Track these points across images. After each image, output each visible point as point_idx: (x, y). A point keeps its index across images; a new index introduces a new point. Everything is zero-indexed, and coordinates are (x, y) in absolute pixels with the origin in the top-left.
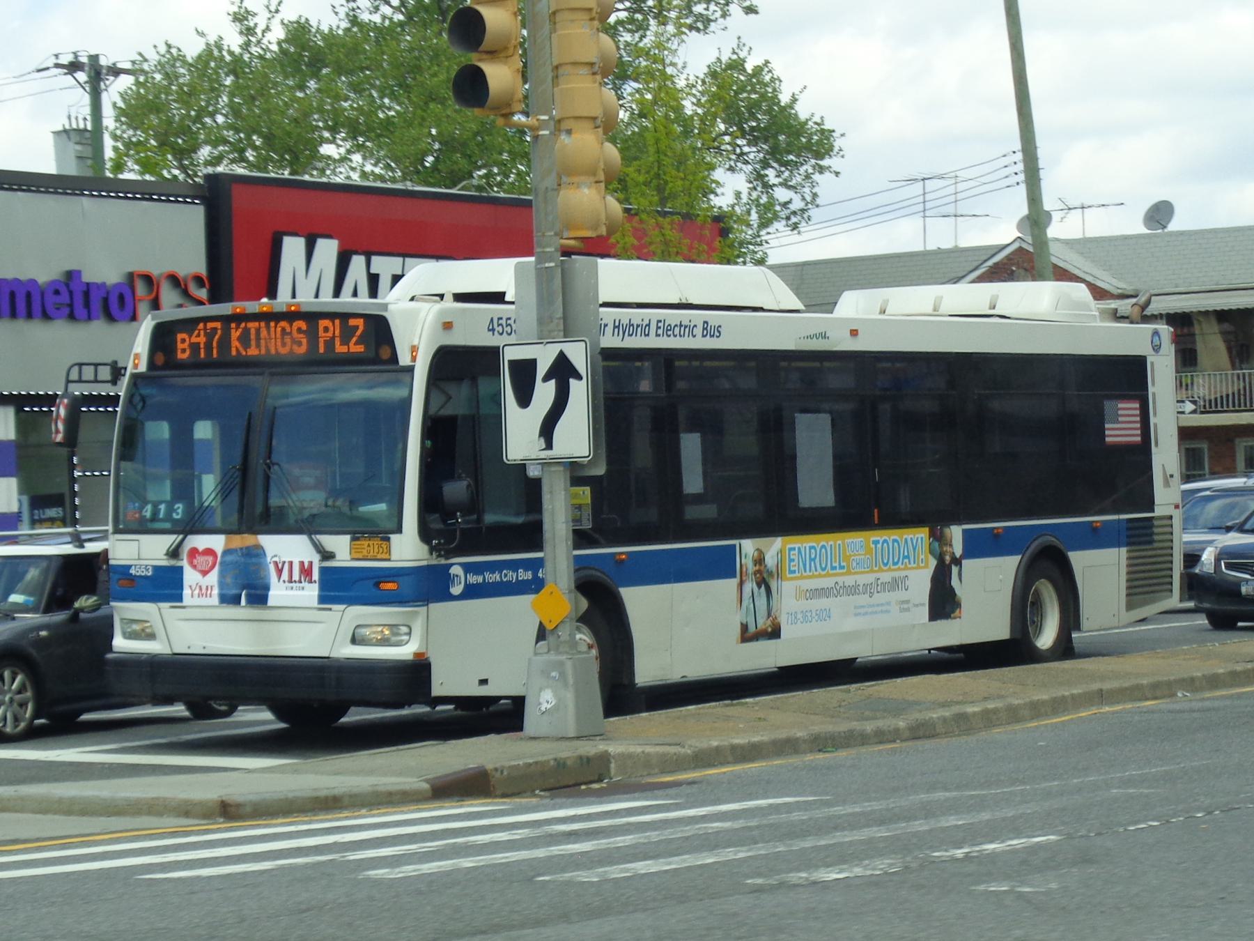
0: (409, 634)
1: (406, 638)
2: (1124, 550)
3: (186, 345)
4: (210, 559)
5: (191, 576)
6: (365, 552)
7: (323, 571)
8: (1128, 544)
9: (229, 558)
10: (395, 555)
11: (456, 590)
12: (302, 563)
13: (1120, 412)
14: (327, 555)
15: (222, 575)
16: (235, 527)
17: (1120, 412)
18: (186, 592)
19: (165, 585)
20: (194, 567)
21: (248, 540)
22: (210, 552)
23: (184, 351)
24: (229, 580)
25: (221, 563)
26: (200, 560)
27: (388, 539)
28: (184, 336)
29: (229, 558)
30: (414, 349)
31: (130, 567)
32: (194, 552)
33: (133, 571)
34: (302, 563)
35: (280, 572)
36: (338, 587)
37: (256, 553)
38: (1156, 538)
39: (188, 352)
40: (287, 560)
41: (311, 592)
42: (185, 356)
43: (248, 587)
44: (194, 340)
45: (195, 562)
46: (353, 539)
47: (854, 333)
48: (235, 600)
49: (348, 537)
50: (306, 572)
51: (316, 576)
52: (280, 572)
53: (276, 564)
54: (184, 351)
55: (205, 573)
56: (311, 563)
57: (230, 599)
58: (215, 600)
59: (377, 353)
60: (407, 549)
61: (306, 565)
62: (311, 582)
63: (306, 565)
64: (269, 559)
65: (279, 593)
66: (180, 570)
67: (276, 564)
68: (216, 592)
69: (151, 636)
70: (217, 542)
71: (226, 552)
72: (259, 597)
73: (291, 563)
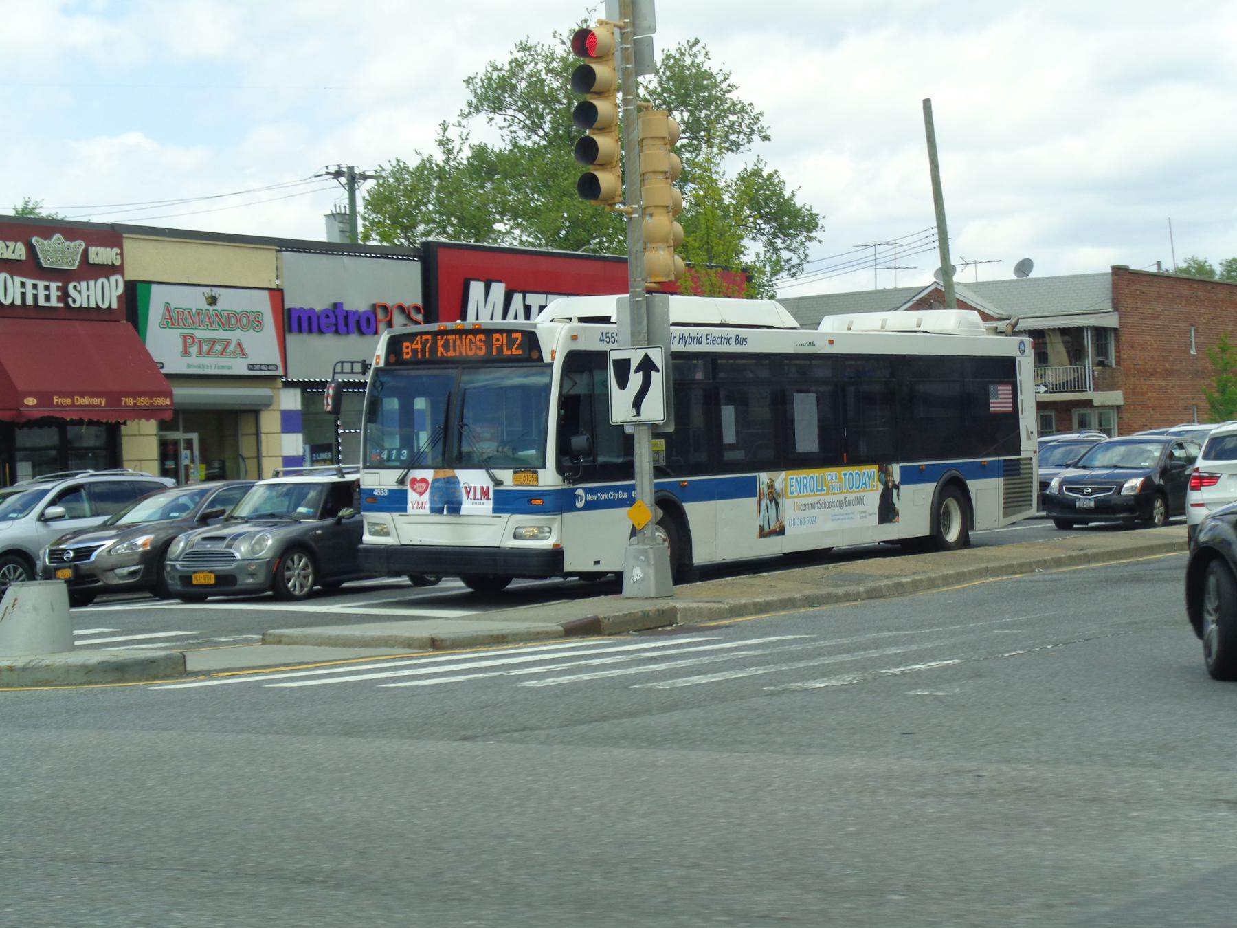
2: (1001, 479)
4: (424, 485)
5: (412, 496)
9: (436, 484)
11: (580, 504)
14: (498, 483)
15: (432, 495)
18: (409, 506)
19: (396, 502)
21: (448, 473)
22: (424, 480)
24: (436, 498)
26: (417, 485)
29: (436, 484)
30: (553, 352)
32: (414, 481)
35: (468, 493)
36: (505, 502)
37: (453, 481)
41: (488, 506)
43: (448, 502)
44: (414, 346)
48: (440, 511)
50: (485, 493)
51: (491, 495)
52: (468, 493)
55: (421, 494)
57: (437, 510)
58: (427, 511)
60: (549, 478)
65: (467, 506)
68: (428, 506)
69: (387, 534)
70: (429, 474)
71: (434, 481)
72: (455, 509)
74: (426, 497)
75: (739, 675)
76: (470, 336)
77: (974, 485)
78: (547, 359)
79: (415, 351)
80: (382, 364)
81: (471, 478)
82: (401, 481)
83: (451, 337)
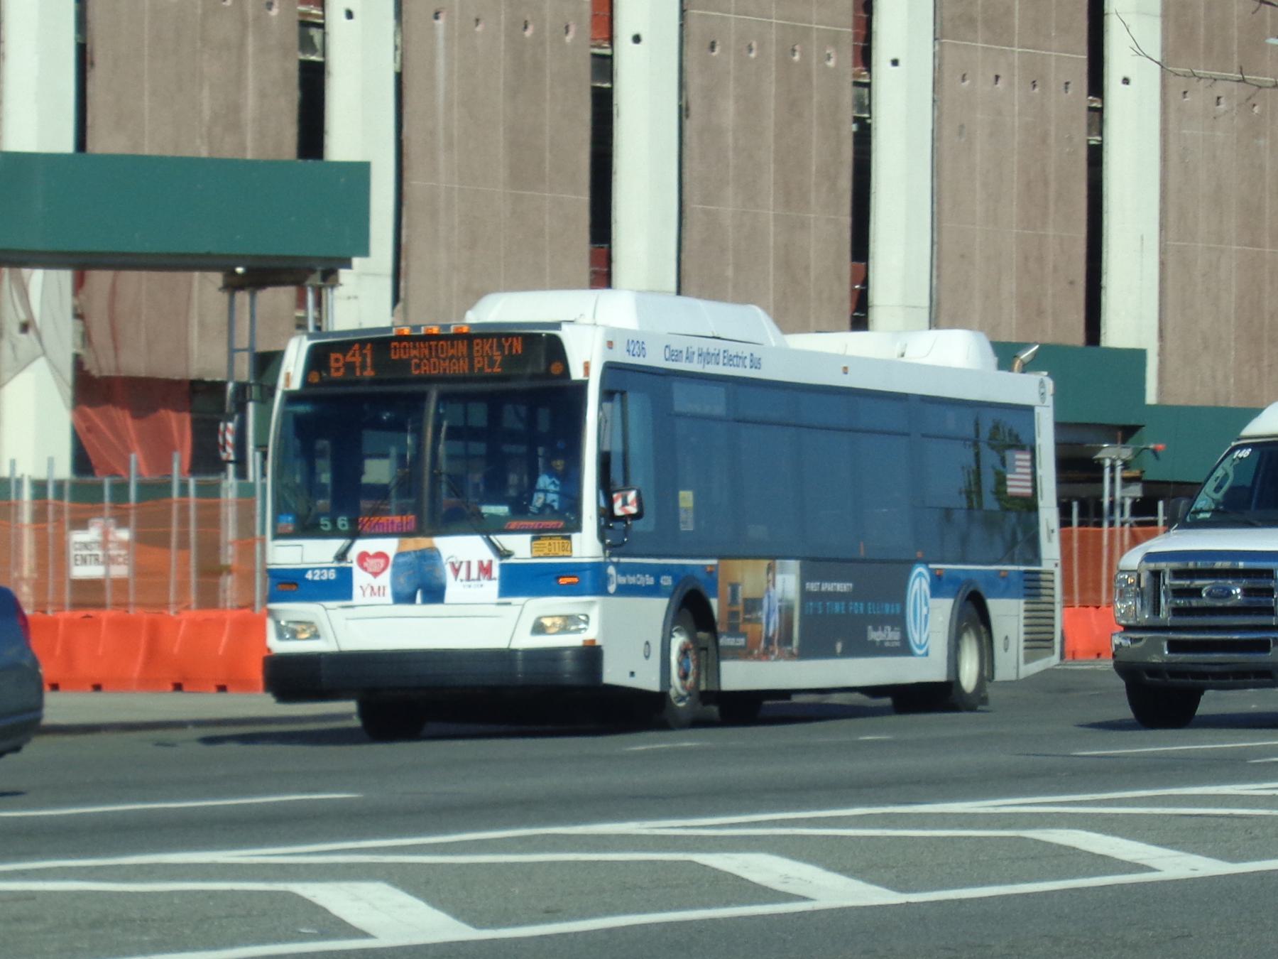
0: (587, 622)
1: (583, 626)
2: (1022, 601)
3: (340, 364)
4: (382, 561)
5: (360, 578)
6: (546, 551)
7: (503, 567)
8: (1026, 596)
9: (401, 560)
10: (576, 552)
11: (612, 588)
12: (481, 563)
13: (1018, 463)
14: (502, 553)
15: (395, 577)
16: (412, 526)
17: (1018, 463)
18: (357, 591)
19: (338, 587)
20: (365, 569)
21: (422, 543)
22: (381, 555)
23: (337, 369)
24: (402, 580)
25: (394, 566)
26: (370, 563)
27: (569, 538)
28: (339, 356)
29: (401, 560)
30: (587, 367)
31: (305, 571)
32: (363, 557)
33: (309, 576)
34: (481, 563)
35: (456, 571)
36: (519, 581)
37: (429, 558)
38: (1043, 591)
39: (342, 370)
40: (465, 559)
41: (491, 587)
42: (340, 374)
43: (424, 585)
44: (349, 358)
45: (365, 564)
46: (534, 539)
47: (845, 370)
48: (411, 599)
49: (527, 538)
50: (485, 570)
51: (496, 572)
52: (456, 571)
53: (453, 564)
54: (337, 369)
55: (375, 574)
56: (490, 562)
57: (403, 597)
58: (389, 598)
59: (548, 369)
60: (586, 545)
61: (485, 563)
62: (490, 578)
63: (485, 563)
64: (444, 560)
65: (454, 589)
66: (349, 570)
67: (453, 564)
68: (389, 591)
69: (315, 636)
70: (390, 546)
71: (399, 554)
72: (435, 594)
73: (469, 563)
74: (385, 579)
75: (1236, 637)
76: (405, 343)
77: (995, 606)
78: (577, 374)
79: (350, 367)
80: (296, 385)
81: (460, 549)
82: (342, 556)
83: (433, 343)
